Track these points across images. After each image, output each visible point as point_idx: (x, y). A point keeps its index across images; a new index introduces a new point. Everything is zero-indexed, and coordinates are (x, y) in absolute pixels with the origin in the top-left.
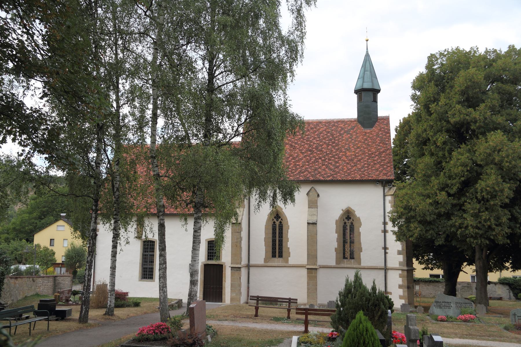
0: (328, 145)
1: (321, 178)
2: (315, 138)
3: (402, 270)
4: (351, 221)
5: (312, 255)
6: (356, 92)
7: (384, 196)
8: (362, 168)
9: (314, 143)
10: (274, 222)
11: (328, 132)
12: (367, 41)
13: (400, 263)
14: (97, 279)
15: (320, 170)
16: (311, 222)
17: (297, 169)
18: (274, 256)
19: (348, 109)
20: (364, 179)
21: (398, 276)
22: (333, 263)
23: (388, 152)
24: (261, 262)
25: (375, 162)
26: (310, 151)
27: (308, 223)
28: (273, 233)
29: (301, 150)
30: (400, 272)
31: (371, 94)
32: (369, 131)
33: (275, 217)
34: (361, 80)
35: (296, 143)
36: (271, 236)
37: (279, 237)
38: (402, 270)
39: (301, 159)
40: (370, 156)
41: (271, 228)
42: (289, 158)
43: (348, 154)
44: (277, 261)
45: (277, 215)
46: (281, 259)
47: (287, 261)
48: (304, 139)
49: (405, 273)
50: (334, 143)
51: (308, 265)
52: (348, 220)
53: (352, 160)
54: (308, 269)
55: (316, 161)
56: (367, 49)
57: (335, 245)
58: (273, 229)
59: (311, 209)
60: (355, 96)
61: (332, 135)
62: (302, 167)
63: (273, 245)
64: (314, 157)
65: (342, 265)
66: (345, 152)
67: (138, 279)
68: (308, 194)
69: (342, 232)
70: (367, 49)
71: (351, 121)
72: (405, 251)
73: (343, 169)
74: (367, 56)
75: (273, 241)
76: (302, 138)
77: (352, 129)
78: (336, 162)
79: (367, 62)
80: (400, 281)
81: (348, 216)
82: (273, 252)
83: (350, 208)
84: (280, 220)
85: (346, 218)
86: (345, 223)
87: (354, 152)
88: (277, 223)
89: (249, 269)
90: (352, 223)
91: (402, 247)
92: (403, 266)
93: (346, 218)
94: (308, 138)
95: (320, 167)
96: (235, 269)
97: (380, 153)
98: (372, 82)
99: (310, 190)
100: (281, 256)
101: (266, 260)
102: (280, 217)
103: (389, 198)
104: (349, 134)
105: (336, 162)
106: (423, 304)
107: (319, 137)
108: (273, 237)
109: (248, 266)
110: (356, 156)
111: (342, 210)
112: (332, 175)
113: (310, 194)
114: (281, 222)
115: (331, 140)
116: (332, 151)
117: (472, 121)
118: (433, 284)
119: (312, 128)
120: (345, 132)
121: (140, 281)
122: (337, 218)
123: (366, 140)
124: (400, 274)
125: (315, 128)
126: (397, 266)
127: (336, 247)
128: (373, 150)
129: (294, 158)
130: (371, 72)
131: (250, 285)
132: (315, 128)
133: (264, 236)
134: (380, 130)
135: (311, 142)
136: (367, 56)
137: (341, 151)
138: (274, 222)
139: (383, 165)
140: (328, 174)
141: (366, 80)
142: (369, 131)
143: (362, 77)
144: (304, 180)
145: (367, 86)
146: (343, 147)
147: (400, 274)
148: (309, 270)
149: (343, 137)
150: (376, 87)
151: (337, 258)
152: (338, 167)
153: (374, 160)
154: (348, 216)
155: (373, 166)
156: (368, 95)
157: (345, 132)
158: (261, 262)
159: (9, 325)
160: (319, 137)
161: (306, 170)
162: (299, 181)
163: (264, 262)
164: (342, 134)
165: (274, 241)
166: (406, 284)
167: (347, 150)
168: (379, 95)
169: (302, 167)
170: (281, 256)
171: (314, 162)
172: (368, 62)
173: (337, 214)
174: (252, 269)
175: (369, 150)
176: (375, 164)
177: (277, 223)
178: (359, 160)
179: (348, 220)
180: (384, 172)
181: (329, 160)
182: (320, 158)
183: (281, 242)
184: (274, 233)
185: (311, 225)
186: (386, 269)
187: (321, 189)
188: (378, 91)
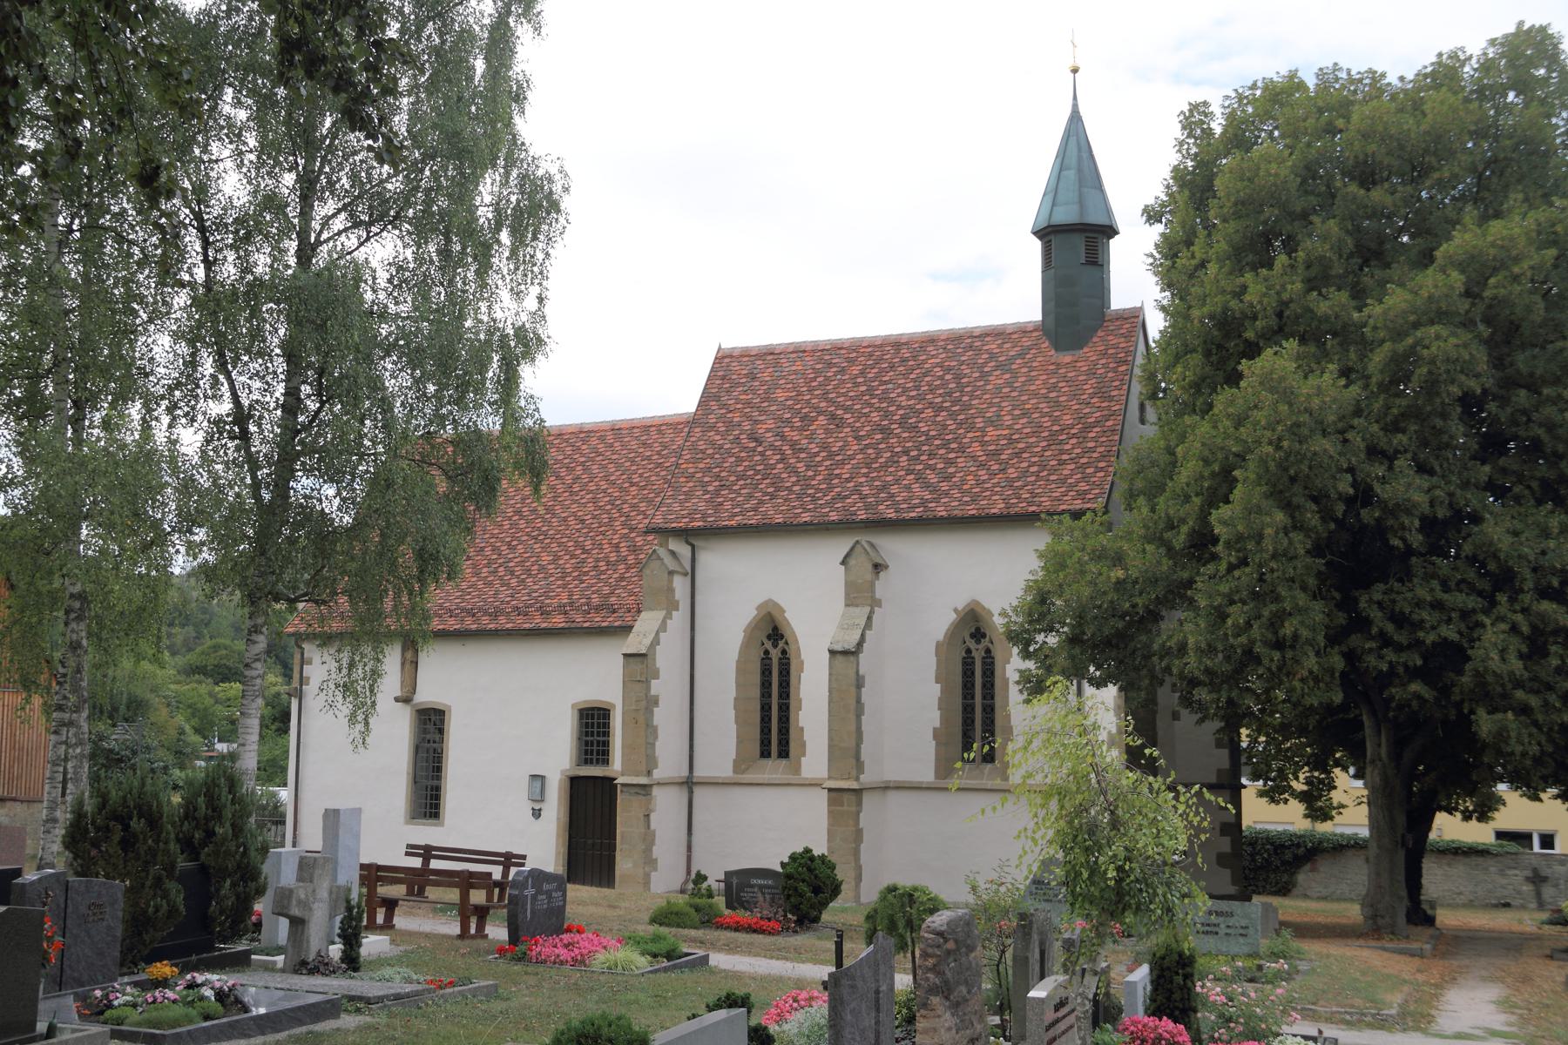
0: (939, 409)
1: (891, 514)
2: (905, 390)
4: (985, 643)
5: (848, 748)
8: (1019, 478)
9: (899, 407)
10: (767, 652)
11: (950, 369)
12: (1075, 71)
15: (894, 489)
16: (838, 647)
17: (831, 488)
18: (765, 754)
19: (1015, 294)
20: (1013, 511)
22: (927, 775)
23: (1110, 423)
24: (725, 770)
25: (1065, 457)
26: (882, 431)
27: (832, 652)
28: (763, 684)
29: (858, 430)
31: (1079, 241)
32: (1068, 359)
33: (769, 637)
34: (1051, 196)
35: (847, 409)
36: (756, 692)
37: (780, 696)
39: (852, 457)
40: (1053, 439)
41: (756, 667)
42: (816, 455)
43: (992, 433)
44: (773, 769)
45: (775, 629)
46: (784, 762)
47: (797, 770)
48: (873, 396)
50: (954, 403)
51: (830, 778)
52: (978, 642)
53: (997, 453)
54: (830, 790)
55: (894, 460)
56: (1075, 97)
57: (934, 718)
58: (763, 673)
59: (851, 609)
60: (1037, 245)
61: (958, 377)
62: (848, 480)
63: (762, 719)
64: (890, 448)
65: (747, 777)
66: (982, 430)
67: (402, 820)
68: (843, 563)
69: (959, 679)
70: (1075, 97)
71: (1023, 330)
73: (963, 481)
74: (1075, 119)
75: (762, 708)
76: (870, 390)
77: (1021, 355)
78: (950, 462)
81: (978, 629)
82: (762, 742)
83: (978, 603)
84: (781, 644)
85: (972, 636)
86: (969, 651)
87: (1009, 427)
88: (775, 654)
89: (691, 792)
90: (988, 651)
93: (972, 636)
94: (885, 392)
95: (897, 482)
96: (633, 790)
97: (1087, 428)
98: (1081, 202)
99: (852, 549)
100: (784, 753)
101: (738, 766)
102: (782, 637)
104: (1010, 371)
105: (950, 462)
107: (917, 388)
108: (763, 695)
109: (689, 784)
110: (1011, 441)
111: (956, 610)
112: (924, 503)
113: (852, 562)
114: (784, 652)
115: (950, 394)
116: (945, 427)
117: (1247, 317)
118: (1467, 860)
119: (904, 360)
120: (997, 368)
121: (407, 823)
122: (940, 636)
123: (1054, 387)
125: (914, 358)
127: (938, 725)
128: (1068, 419)
129: (831, 456)
130: (1080, 171)
131: (695, 838)
132: (914, 358)
133: (734, 694)
134: (1104, 354)
135: (892, 402)
136: (1075, 119)
137: (972, 428)
138: (767, 652)
139: (1085, 466)
140: (910, 497)
141: (1061, 197)
142: (1068, 359)
143: (1054, 193)
144: (840, 522)
145: (1064, 216)
146: (981, 413)
148: (834, 794)
149: (988, 382)
150: (1095, 218)
151: (937, 760)
152: (948, 478)
153: (1062, 452)
154: (978, 629)
155: (1053, 471)
156: (1074, 242)
157: (997, 368)
158: (725, 770)
159: (1315, 1033)
160: (917, 388)
161: (856, 491)
162: (824, 523)
163: (735, 772)
164: (989, 374)
165: (765, 709)
167: (990, 422)
168: (1114, 243)
169: (848, 480)
170: (784, 753)
171: (885, 466)
172: (1073, 140)
173: (940, 622)
174: (698, 791)
175: (1056, 421)
176: (1062, 463)
177: (775, 654)
178: (1018, 455)
179: (978, 642)
180: (1083, 486)
181: (931, 455)
182: (906, 452)
183: (785, 710)
184: (766, 685)
185: (840, 658)
186: (689, 784)
187: (893, 547)
188: (1110, 231)
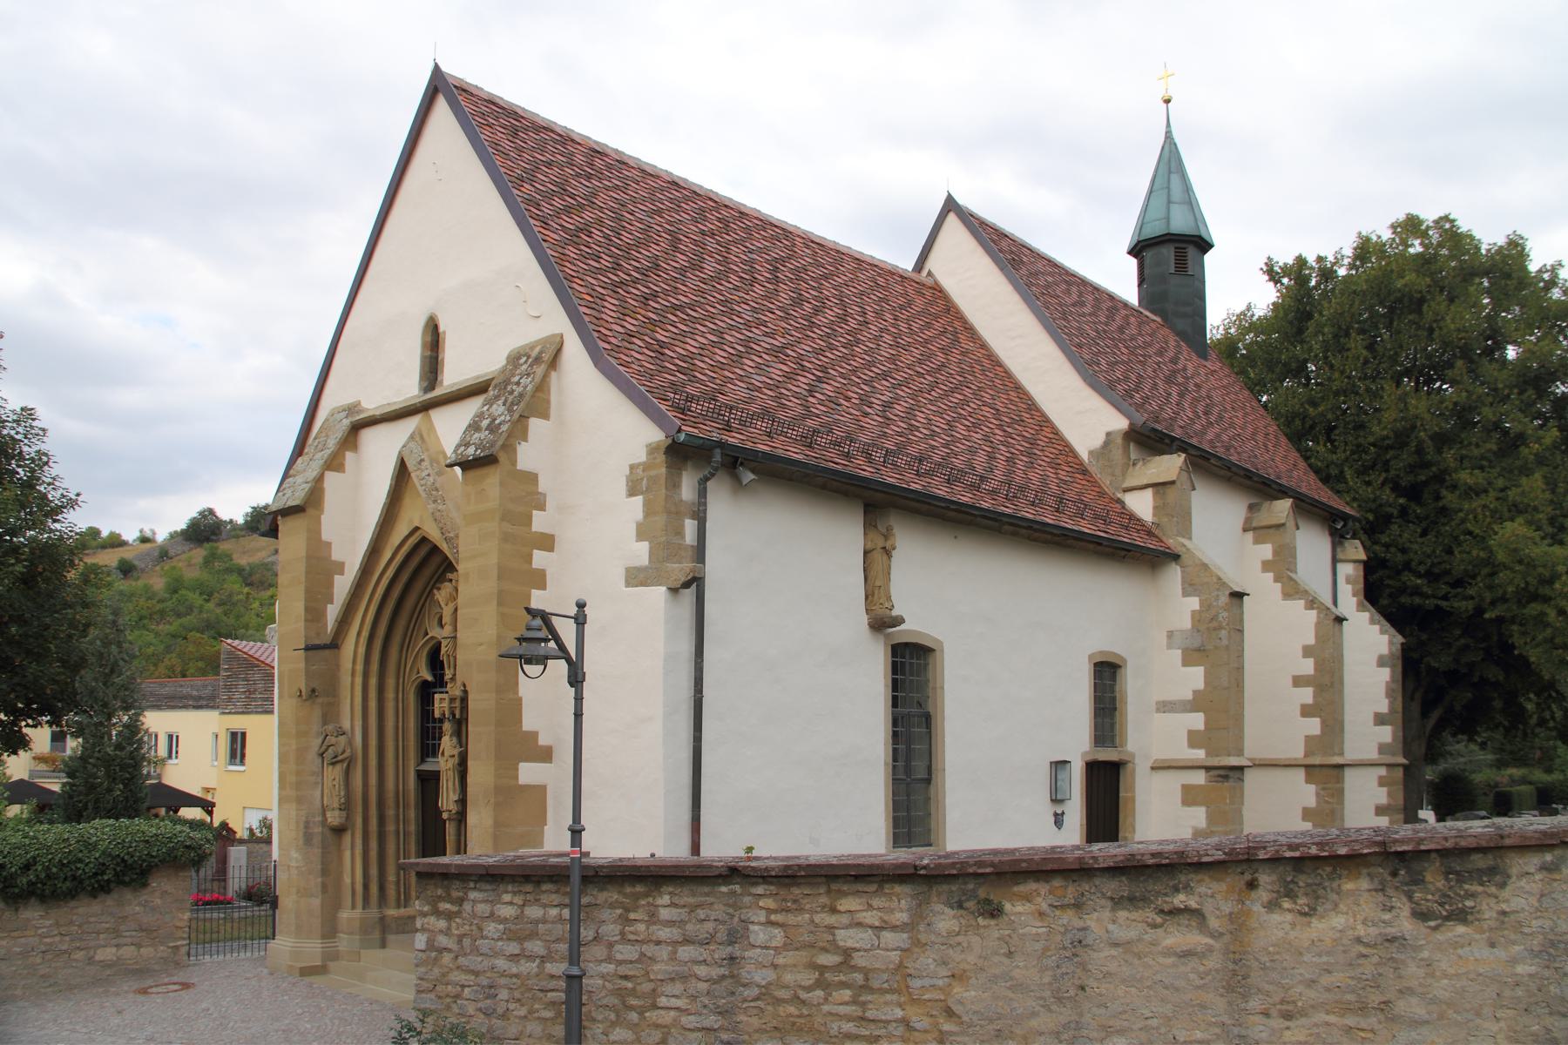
3: (1389, 766)
6: (1136, 251)
7: (1335, 561)
12: (1167, 101)
13: (1382, 748)
14: (883, 851)
21: (1375, 783)
30: (1383, 771)
38: (1389, 766)
49: (1399, 773)
60: (1133, 262)
72: (1399, 716)
79: (1170, 163)
80: (1381, 796)
91: (1391, 704)
92: (1394, 755)
103: (1346, 570)
106: (1317, 840)
124: (542, 585)
126: (1373, 755)
147: (542, 585)
150: (1180, 223)
166: (1400, 800)
